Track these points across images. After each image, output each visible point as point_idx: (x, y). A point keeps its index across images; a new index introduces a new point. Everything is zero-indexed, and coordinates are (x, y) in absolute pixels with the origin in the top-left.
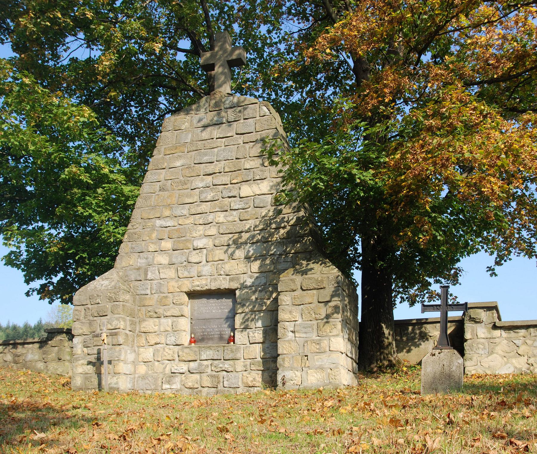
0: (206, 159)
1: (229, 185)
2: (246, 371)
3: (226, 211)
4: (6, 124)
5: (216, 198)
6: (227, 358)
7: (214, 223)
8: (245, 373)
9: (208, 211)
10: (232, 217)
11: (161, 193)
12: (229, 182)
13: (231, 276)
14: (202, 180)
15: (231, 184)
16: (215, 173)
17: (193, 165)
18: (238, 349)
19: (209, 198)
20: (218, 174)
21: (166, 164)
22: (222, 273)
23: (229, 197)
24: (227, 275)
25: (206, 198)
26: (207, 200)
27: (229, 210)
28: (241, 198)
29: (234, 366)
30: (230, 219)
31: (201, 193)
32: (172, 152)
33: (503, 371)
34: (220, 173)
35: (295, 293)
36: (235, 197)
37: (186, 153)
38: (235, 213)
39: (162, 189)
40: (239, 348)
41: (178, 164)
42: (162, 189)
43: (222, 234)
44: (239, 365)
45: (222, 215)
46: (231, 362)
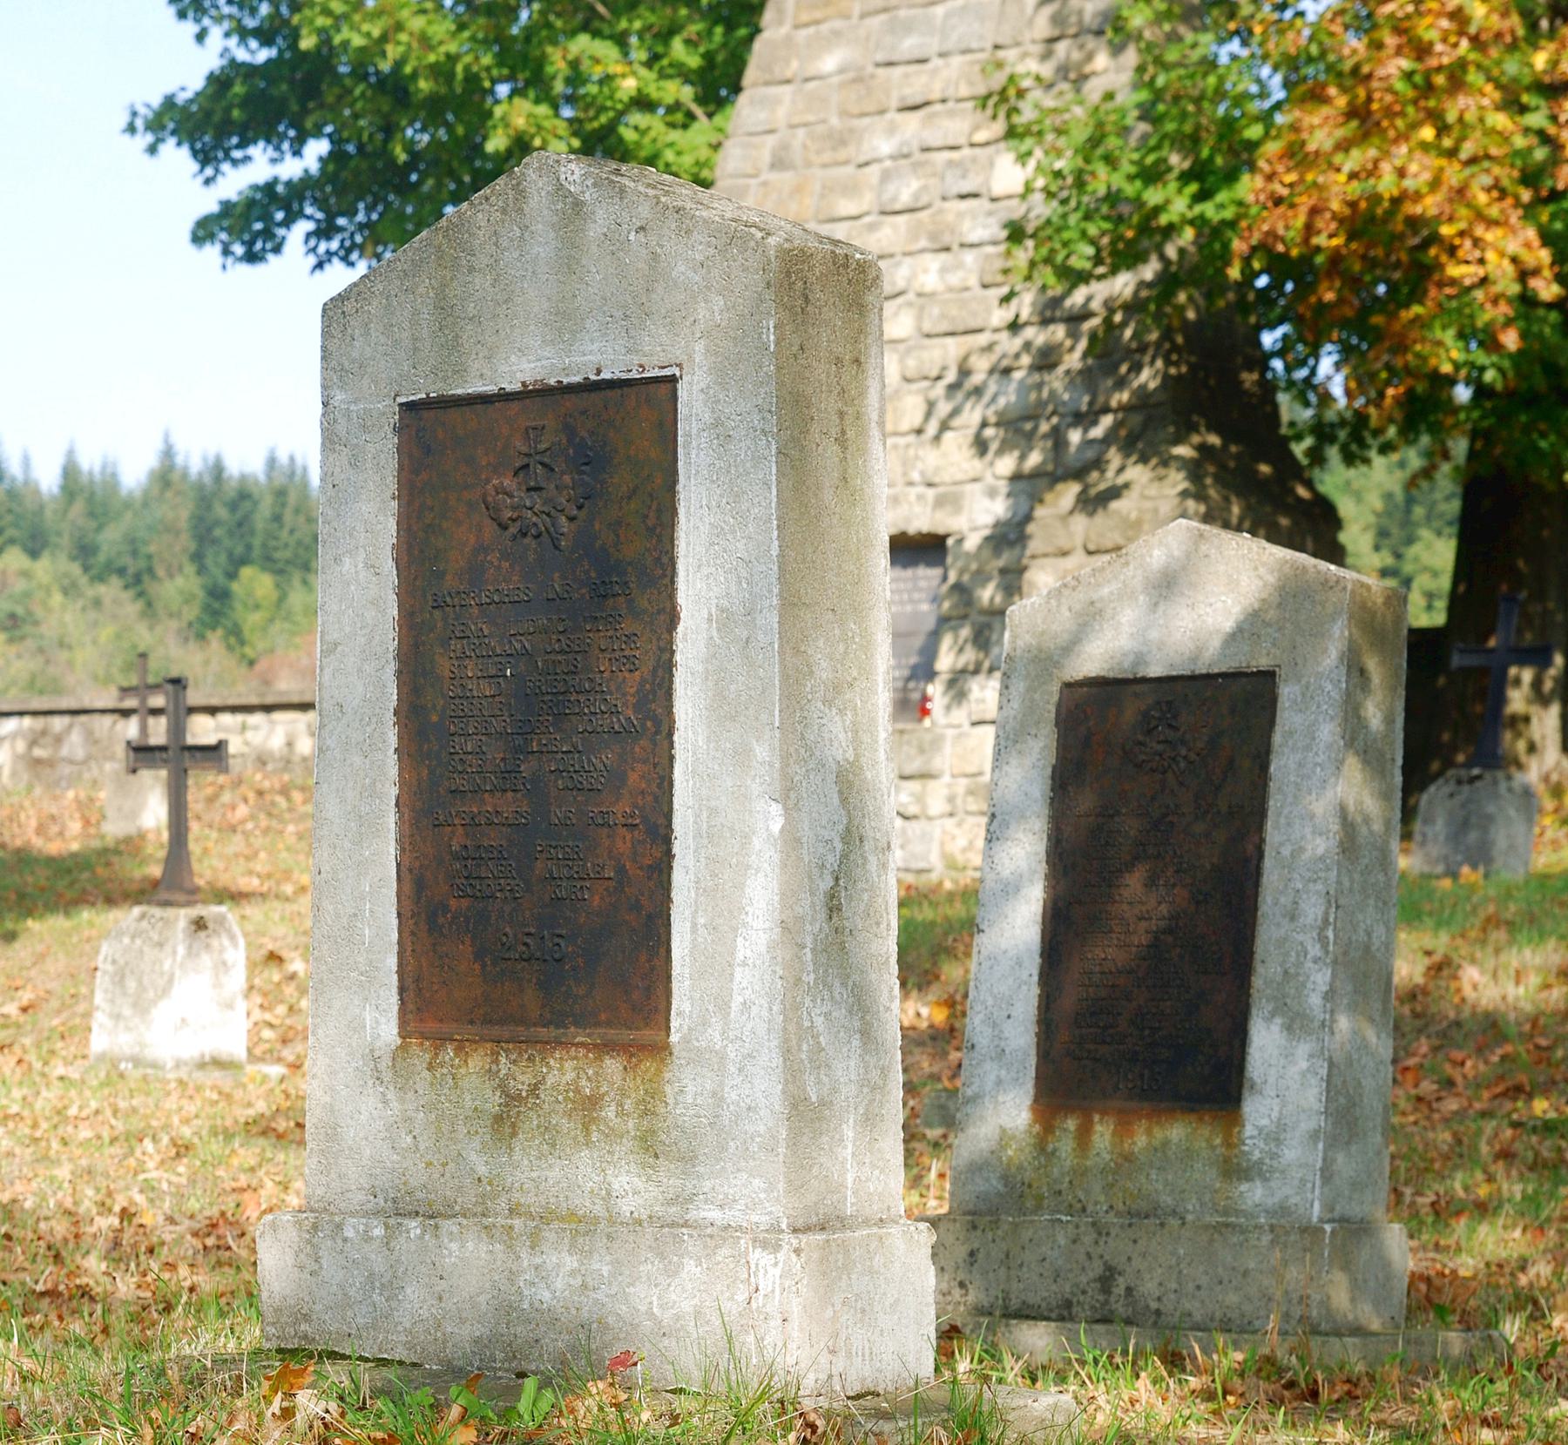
0: (909, 45)
1: (967, 151)
2: (951, 815)
3: (947, 249)
4: (1279, 94)
5: (924, 201)
6: (908, 771)
7: (911, 296)
8: (949, 823)
9: (897, 249)
10: (960, 274)
11: (774, 177)
12: (962, 141)
13: (941, 490)
14: (892, 130)
15: (972, 145)
16: (927, 104)
17: (870, 69)
18: (937, 743)
19: (905, 198)
20: (938, 107)
21: (795, 64)
22: (916, 476)
23: (963, 197)
24: (930, 485)
25: (894, 199)
26: (898, 207)
27: (955, 247)
28: (994, 200)
29: (920, 799)
30: (955, 279)
31: (886, 176)
32: (818, 15)
33: (1315, 1091)
34: (944, 101)
35: (1069, 563)
36: (976, 195)
37: (855, 20)
38: (969, 257)
39: (778, 164)
40: (941, 738)
41: (829, 63)
42: (778, 164)
43: (928, 336)
44: (936, 797)
45: (934, 262)
46: (914, 786)
